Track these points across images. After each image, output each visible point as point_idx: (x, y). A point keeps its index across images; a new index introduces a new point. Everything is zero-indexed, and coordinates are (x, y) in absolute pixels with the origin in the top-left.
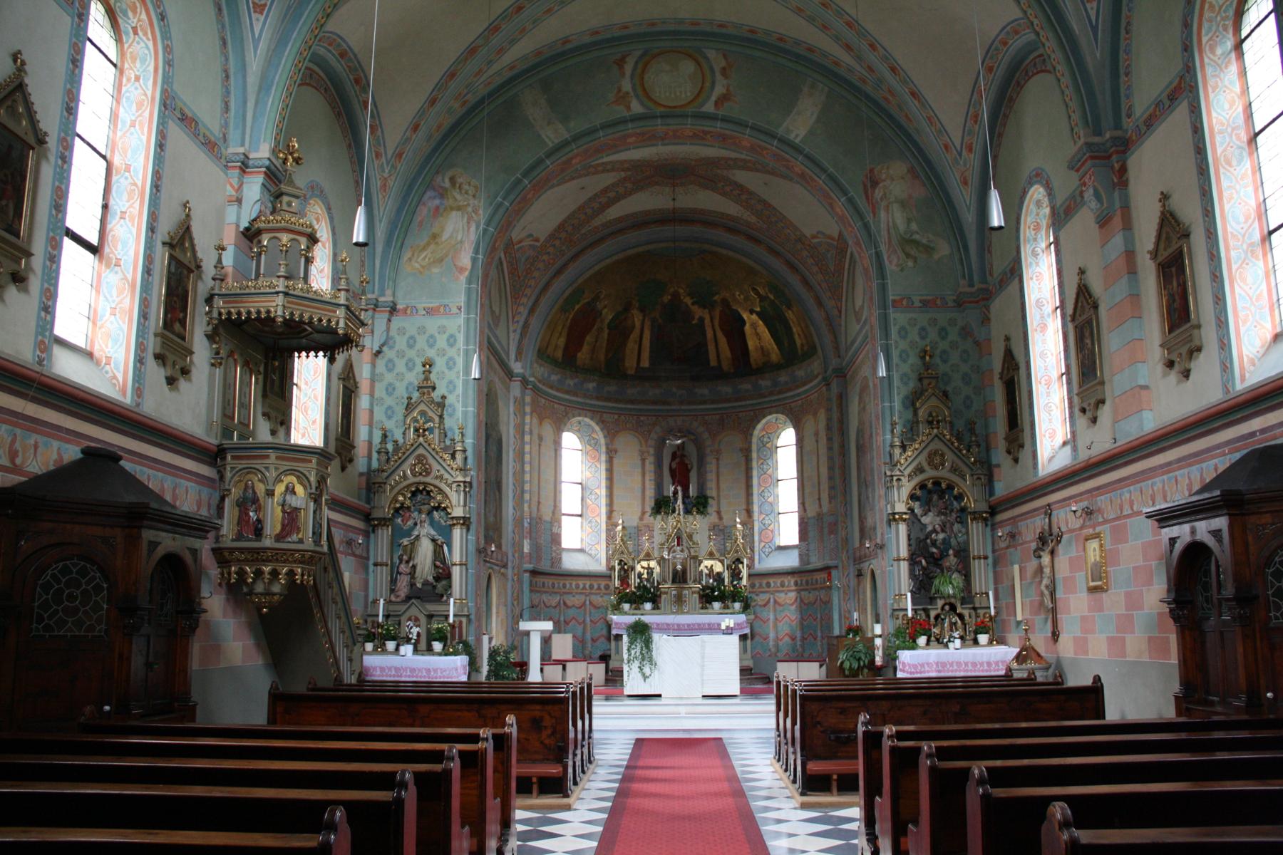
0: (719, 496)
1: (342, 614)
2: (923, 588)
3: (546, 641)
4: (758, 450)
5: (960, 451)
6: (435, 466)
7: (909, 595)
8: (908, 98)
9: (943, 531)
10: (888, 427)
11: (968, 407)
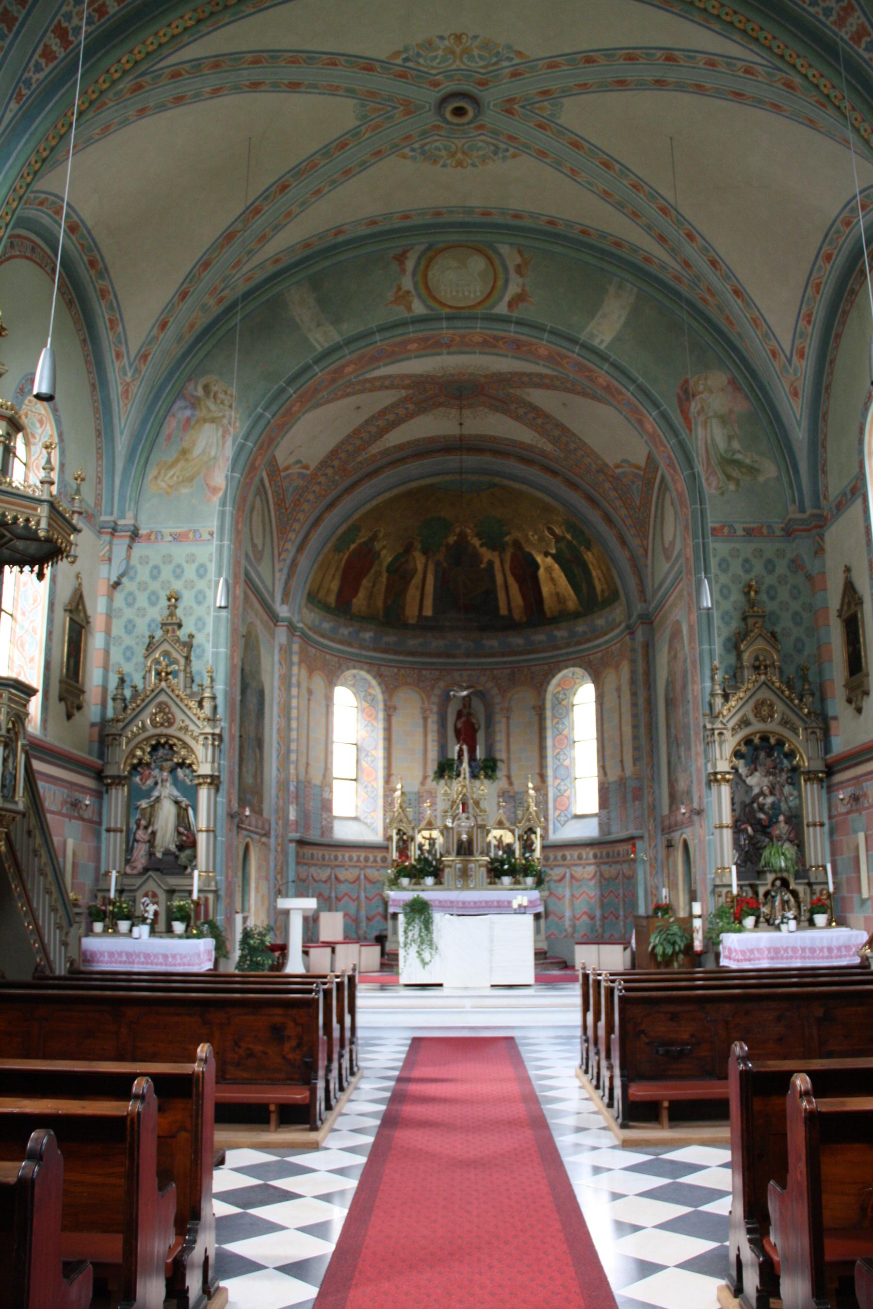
0: (509, 759)
1: (54, 889)
2: (750, 859)
3: (311, 922)
4: (553, 708)
5: (792, 701)
6: (179, 716)
7: (734, 868)
8: (730, 296)
10: (707, 673)
11: (799, 651)
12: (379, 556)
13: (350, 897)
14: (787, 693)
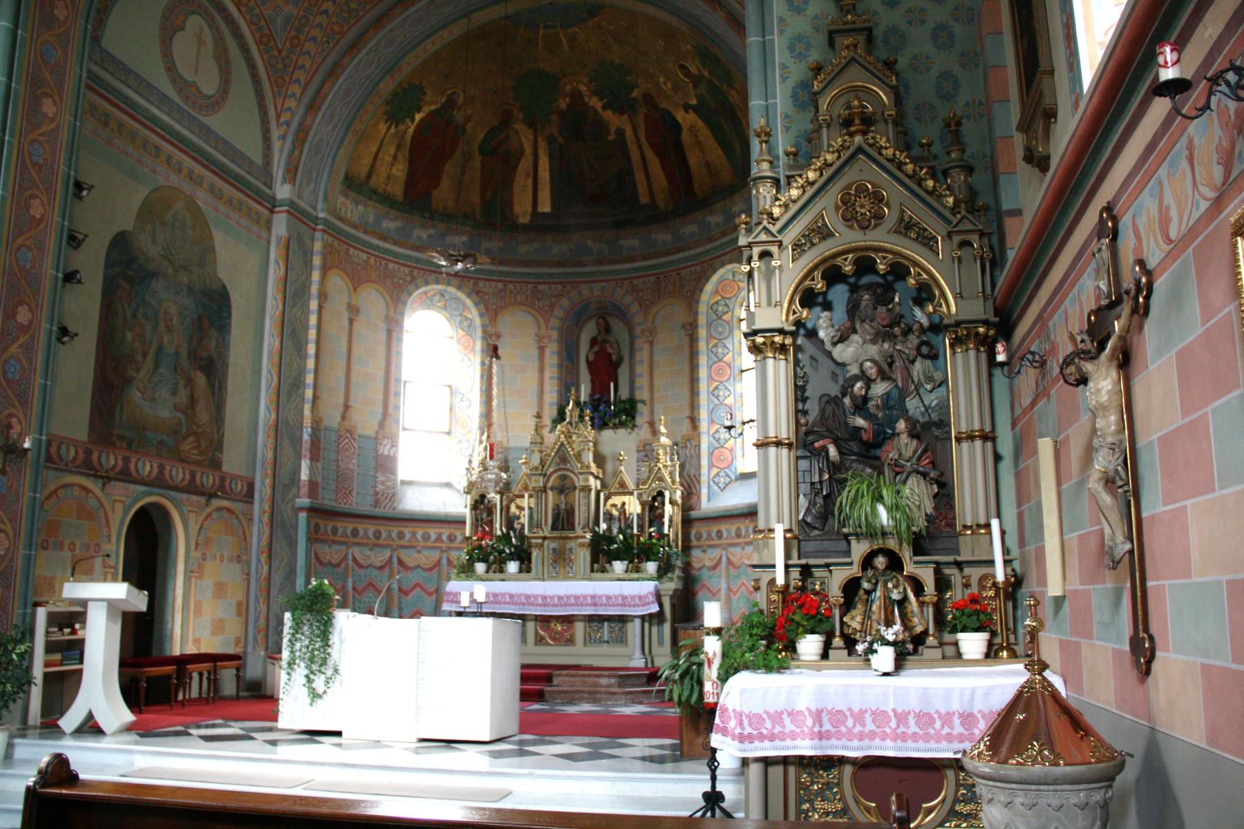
0: (652, 399)
4: (709, 325)
5: (900, 166)
9: (884, 376)
11: (948, 97)
12: (465, 130)
13: (422, 588)
14: (910, 167)
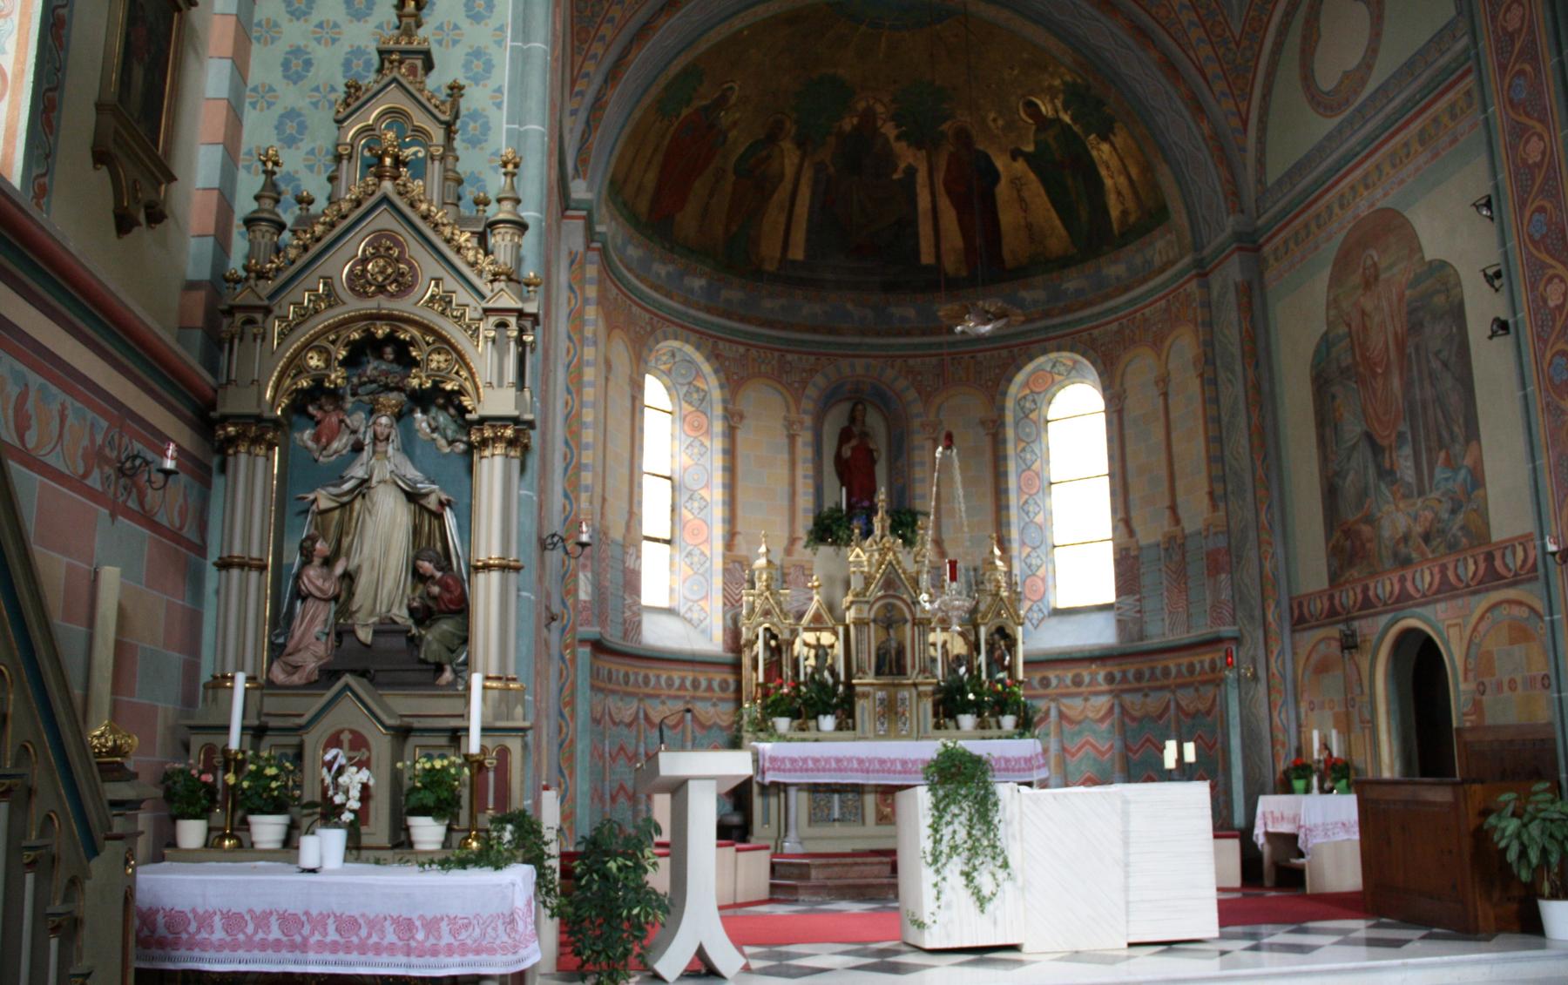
4: (1016, 424)
6: (428, 265)
